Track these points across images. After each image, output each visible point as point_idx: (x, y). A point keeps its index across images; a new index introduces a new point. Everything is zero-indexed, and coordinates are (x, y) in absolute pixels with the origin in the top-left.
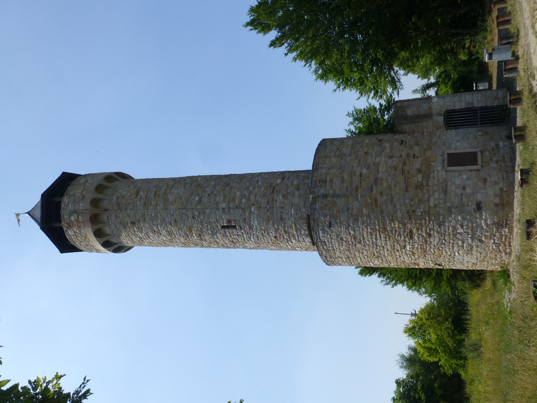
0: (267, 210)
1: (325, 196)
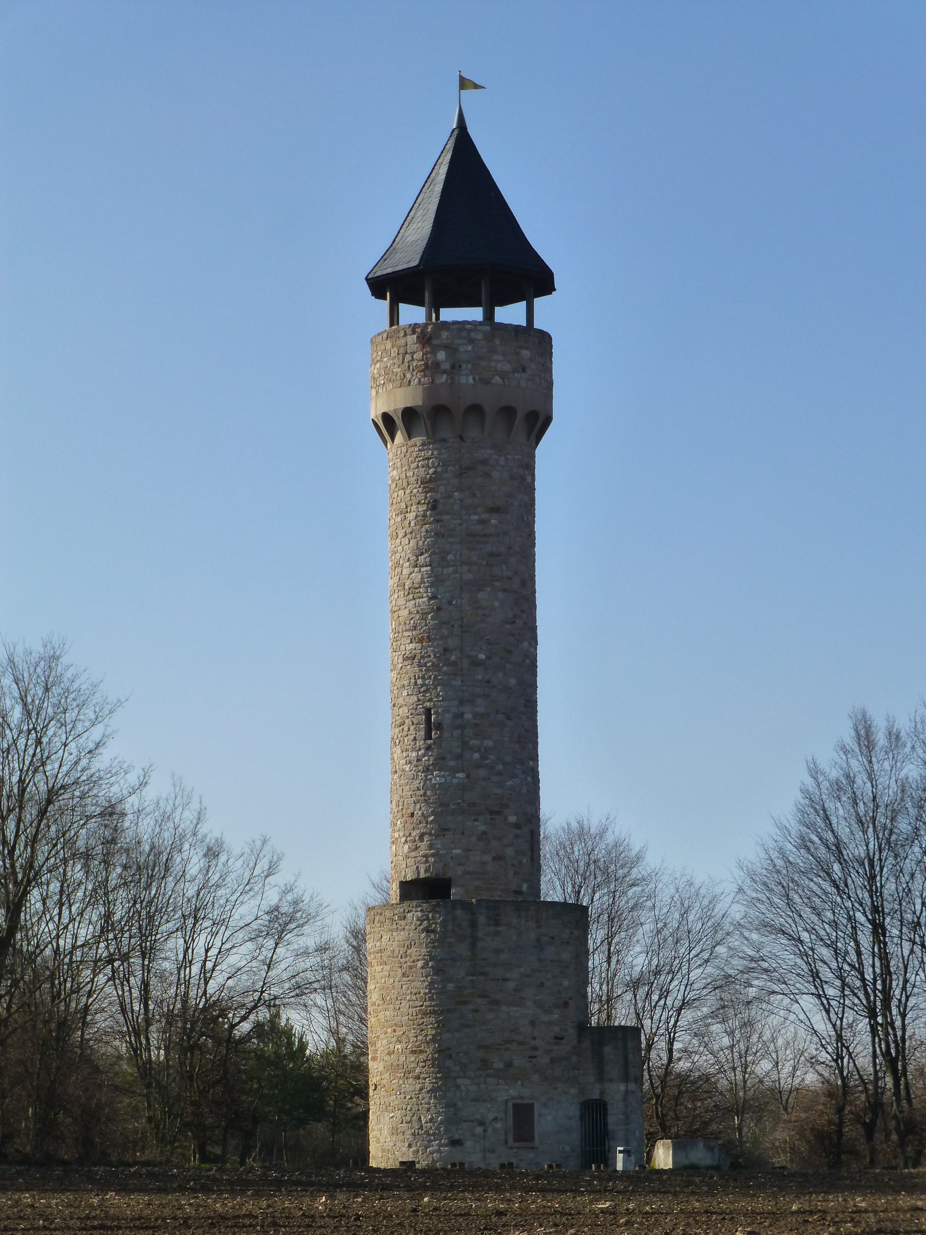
0: (458, 804)
1: (474, 925)
